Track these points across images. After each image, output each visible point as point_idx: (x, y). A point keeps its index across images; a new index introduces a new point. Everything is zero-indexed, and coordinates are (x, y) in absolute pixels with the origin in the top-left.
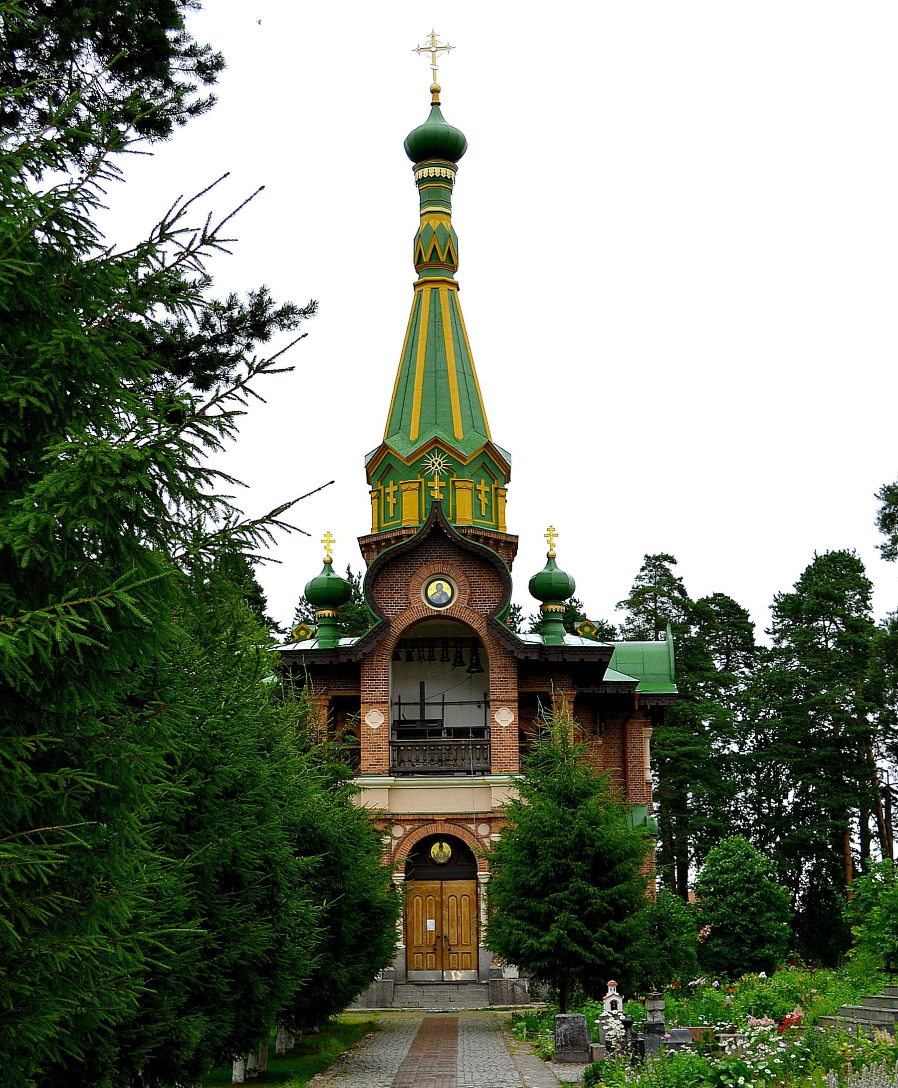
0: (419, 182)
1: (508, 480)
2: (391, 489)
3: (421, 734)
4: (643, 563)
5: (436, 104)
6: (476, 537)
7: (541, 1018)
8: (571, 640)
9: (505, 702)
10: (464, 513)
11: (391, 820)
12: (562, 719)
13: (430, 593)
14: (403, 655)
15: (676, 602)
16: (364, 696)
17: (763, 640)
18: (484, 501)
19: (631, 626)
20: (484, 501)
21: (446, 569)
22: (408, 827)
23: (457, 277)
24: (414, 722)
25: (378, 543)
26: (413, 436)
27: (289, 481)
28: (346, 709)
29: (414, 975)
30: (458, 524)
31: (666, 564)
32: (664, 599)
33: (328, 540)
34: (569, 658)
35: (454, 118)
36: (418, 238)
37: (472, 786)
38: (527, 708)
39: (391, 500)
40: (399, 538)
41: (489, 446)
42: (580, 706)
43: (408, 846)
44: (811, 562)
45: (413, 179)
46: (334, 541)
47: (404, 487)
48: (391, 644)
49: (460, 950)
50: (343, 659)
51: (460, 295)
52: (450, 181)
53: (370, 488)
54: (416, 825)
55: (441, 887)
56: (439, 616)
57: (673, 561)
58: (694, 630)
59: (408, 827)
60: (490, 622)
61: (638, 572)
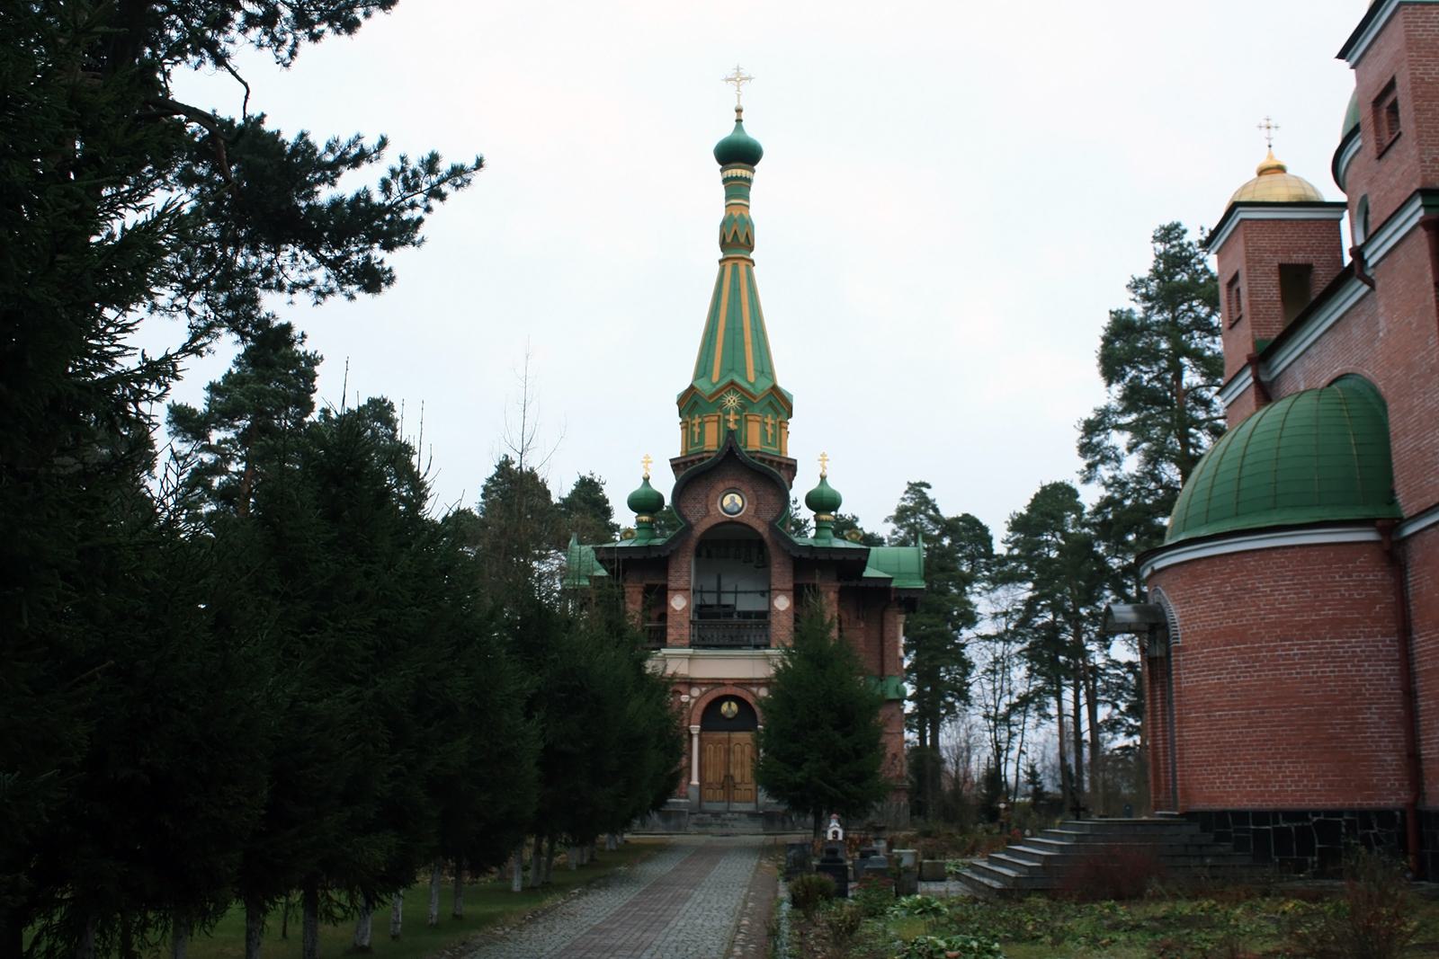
0: (725, 181)
1: (790, 415)
2: (697, 421)
3: (717, 616)
4: (906, 488)
5: (739, 121)
6: (763, 460)
7: (210, 326)
8: (840, 544)
9: (783, 591)
10: (754, 440)
11: (690, 683)
12: (829, 603)
13: (725, 504)
14: (704, 553)
15: (930, 518)
16: (671, 585)
17: (999, 549)
18: (770, 431)
19: (895, 537)
20: (770, 431)
21: (738, 485)
22: (704, 689)
23: (753, 256)
24: (711, 606)
25: (685, 463)
26: (715, 379)
27: (283, 246)
28: (657, 596)
29: (707, 806)
30: (749, 449)
31: (924, 490)
32: (921, 516)
33: (647, 461)
34: (835, 557)
35: (753, 132)
36: (723, 224)
37: (752, 657)
38: (798, 596)
39: (696, 429)
40: (701, 459)
41: (775, 388)
42: (843, 594)
43: (703, 704)
44: (1038, 490)
45: (720, 178)
46: (651, 462)
47: (706, 419)
48: (693, 543)
49: (743, 787)
50: (654, 555)
51: (756, 270)
52: (749, 181)
53: (680, 420)
54: (710, 687)
55: (729, 738)
56: (732, 522)
57: (928, 486)
58: (946, 542)
59: (704, 689)
60: (771, 526)
61: (902, 495)
